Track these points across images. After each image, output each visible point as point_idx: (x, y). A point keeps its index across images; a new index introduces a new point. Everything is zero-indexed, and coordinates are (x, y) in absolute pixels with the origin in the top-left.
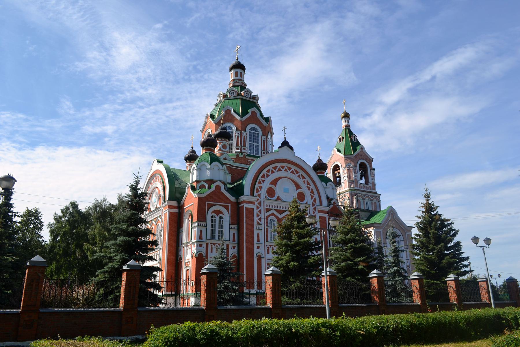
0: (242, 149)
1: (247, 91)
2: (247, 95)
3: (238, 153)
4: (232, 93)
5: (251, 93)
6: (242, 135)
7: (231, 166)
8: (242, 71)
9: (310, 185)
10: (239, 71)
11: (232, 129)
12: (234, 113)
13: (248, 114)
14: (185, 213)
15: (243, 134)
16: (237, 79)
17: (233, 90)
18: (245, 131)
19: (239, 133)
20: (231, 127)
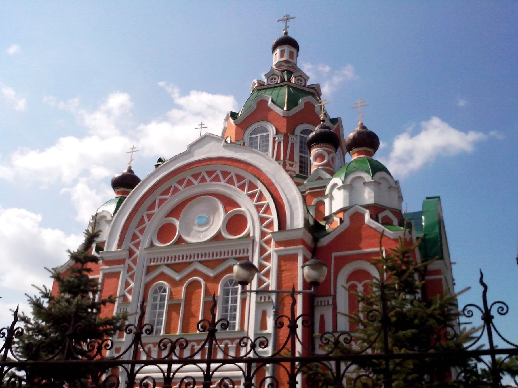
0: (286, 165)
1: (301, 76)
4: (272, 79)
5: (306, 78)
7: (194, 167)
8: (294, 50)
9: (185, 179)
10: (287, 48)
11: (268, 131)
12: (274, 105)
13: (297, 107)
15: (290, 139)
16: (282, 61)
17: (274, 74)
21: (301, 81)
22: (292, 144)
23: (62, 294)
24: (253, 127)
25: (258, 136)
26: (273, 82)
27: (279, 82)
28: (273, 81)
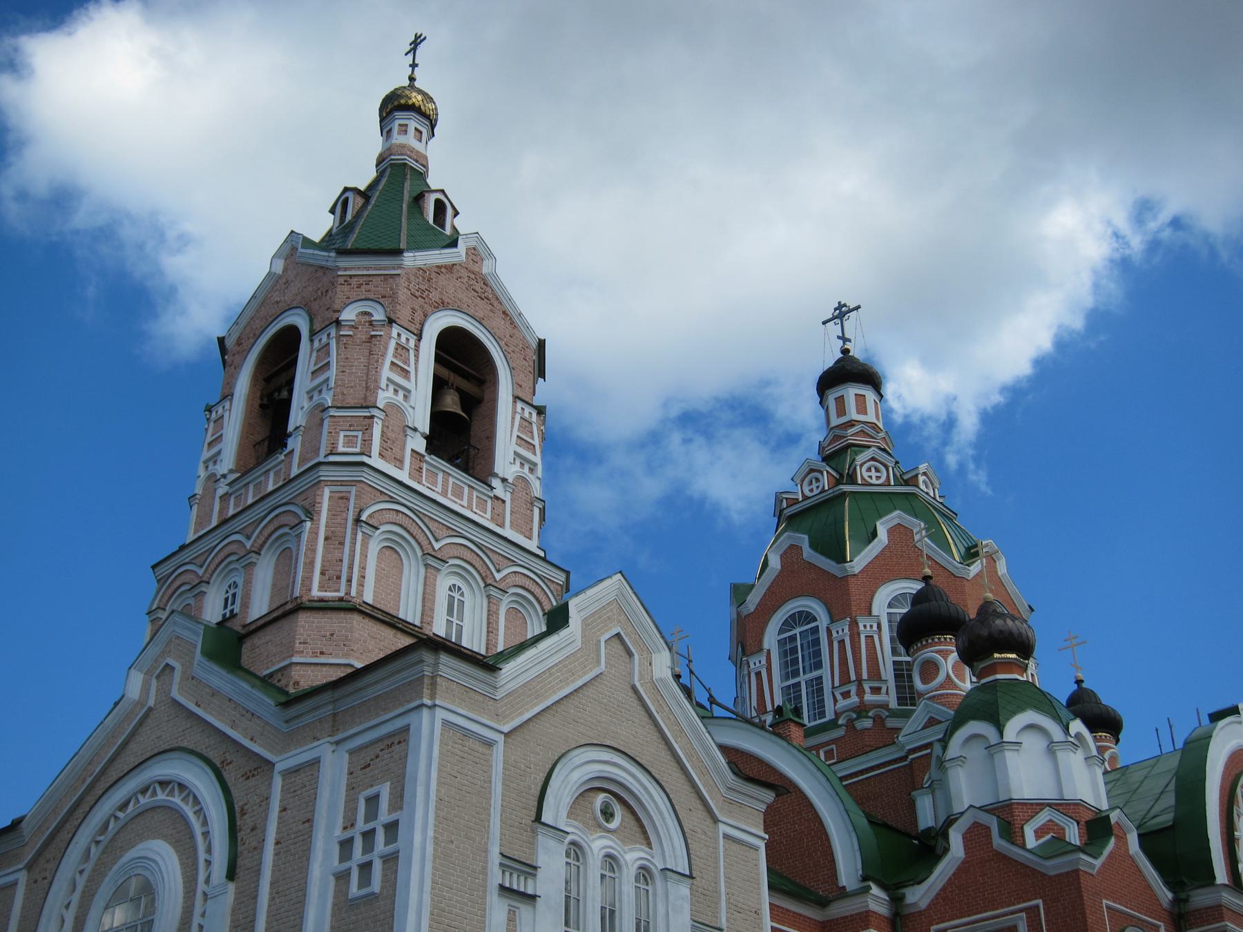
0: (864, 692)
2: (873, 474)
3: (847, 713)
4: (811, 483)
6: (859, 634)
11: (815, 619)
14: (1239, 816)
15: (861, 628)
17: (812, 471)
18: (870, 613)
19: (871, 626)
20: (808, 614)
21: (877, 470)
22: (870, 638)
23: (766, 651)
24: (784, 611)
25: (796, 634)
26: (869, 474)
27: (826, 488)
28: (814, 485)
